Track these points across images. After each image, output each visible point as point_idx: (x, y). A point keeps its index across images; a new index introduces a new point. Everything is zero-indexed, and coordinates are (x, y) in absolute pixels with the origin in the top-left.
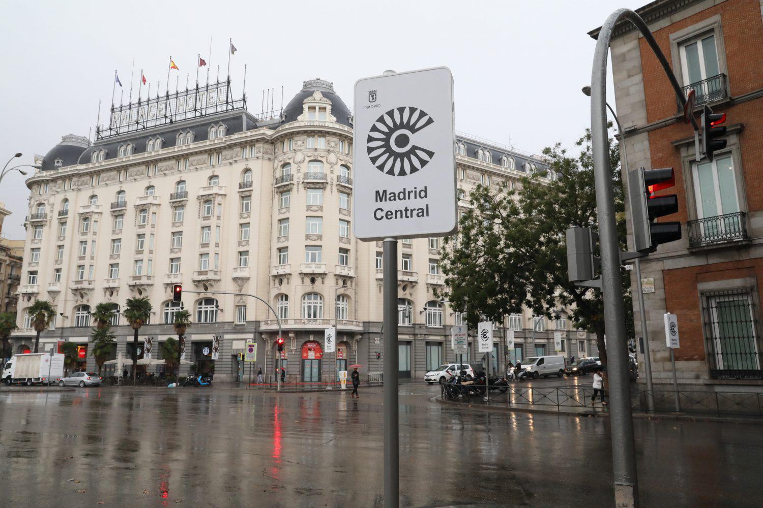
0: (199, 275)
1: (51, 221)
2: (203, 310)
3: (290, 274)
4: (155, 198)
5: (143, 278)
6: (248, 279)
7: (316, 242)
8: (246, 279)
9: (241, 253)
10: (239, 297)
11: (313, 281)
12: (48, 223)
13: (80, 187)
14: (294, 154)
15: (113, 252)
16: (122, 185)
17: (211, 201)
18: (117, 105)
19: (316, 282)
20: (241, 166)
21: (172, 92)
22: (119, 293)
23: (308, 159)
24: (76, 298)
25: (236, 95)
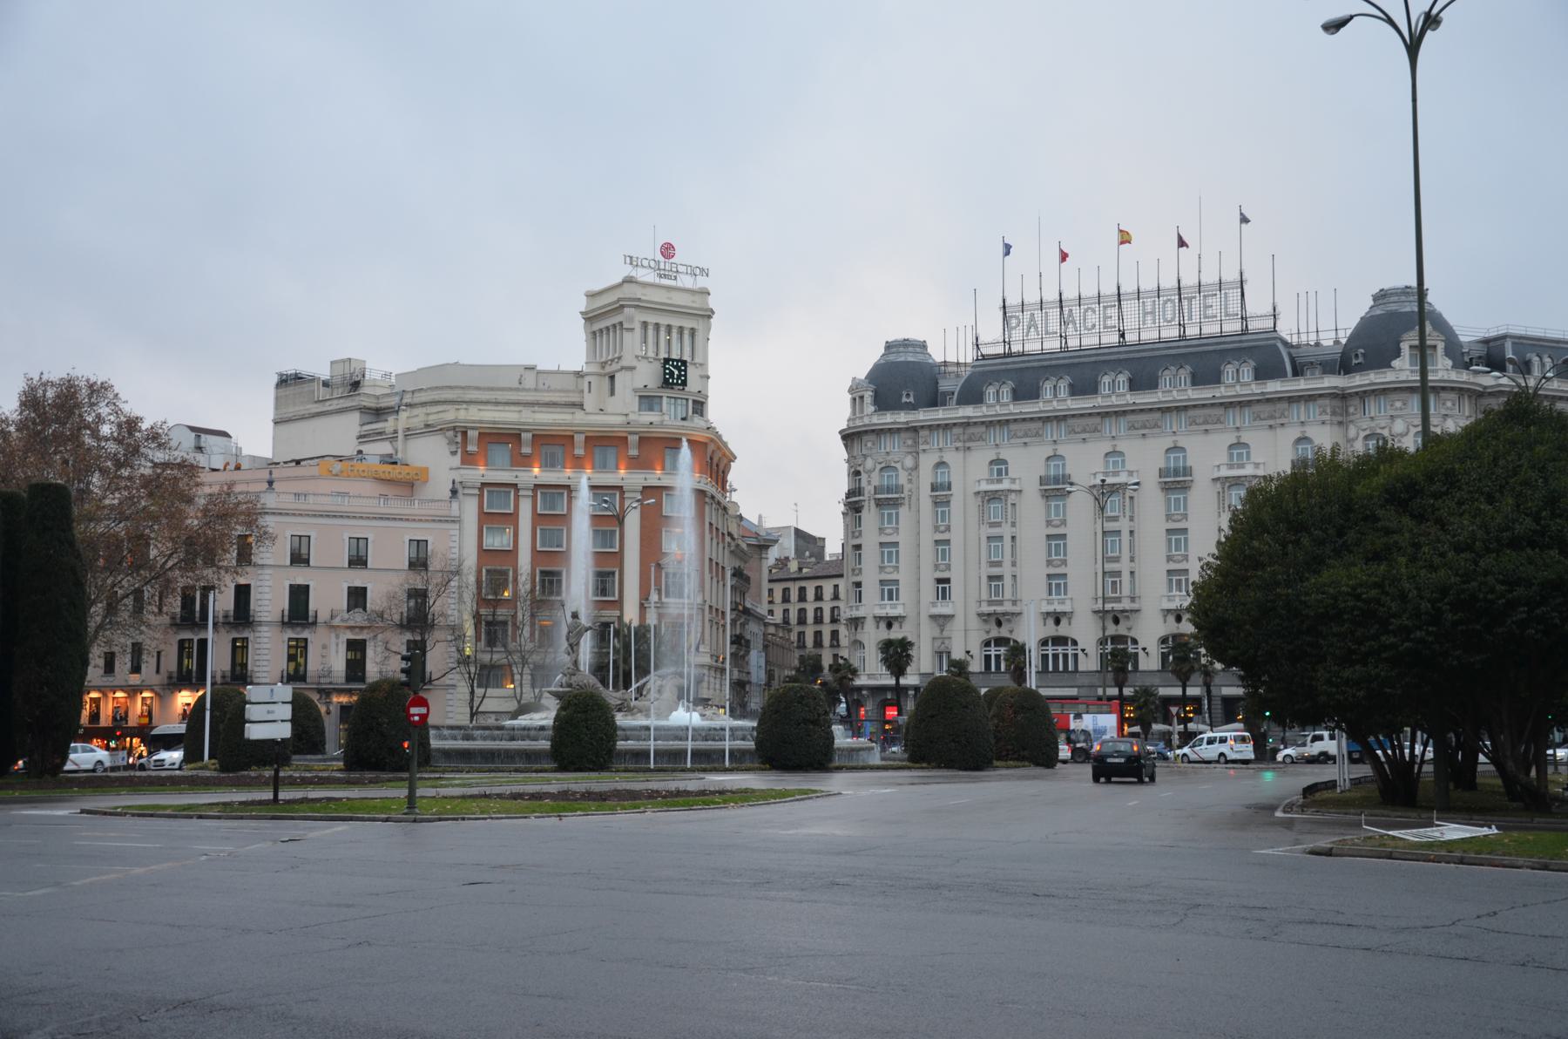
0: (989, 605)
1: (910, 497)
2: (993, 653)
3: (864, 618)
4: (1013, 481)
5: (1006, 603)
6: (952, 616)
7: (1181, 564)
8: (948, 618)
9: (939, 581)
10: (940, 641)
11: (1057, 622)
12: (906, 501)
13: (967, 445)
14: (1390, 421)
15: (883, 561)
16: (943, 454)
17: (1001, 499)
18: (1013, 300)
19: (1061, 623)
20: (1294, 433)
21: (1128, 287)
22: (1073, 621)
23: (879, 467)
24: (987, 627)
25: (1257, 304)
